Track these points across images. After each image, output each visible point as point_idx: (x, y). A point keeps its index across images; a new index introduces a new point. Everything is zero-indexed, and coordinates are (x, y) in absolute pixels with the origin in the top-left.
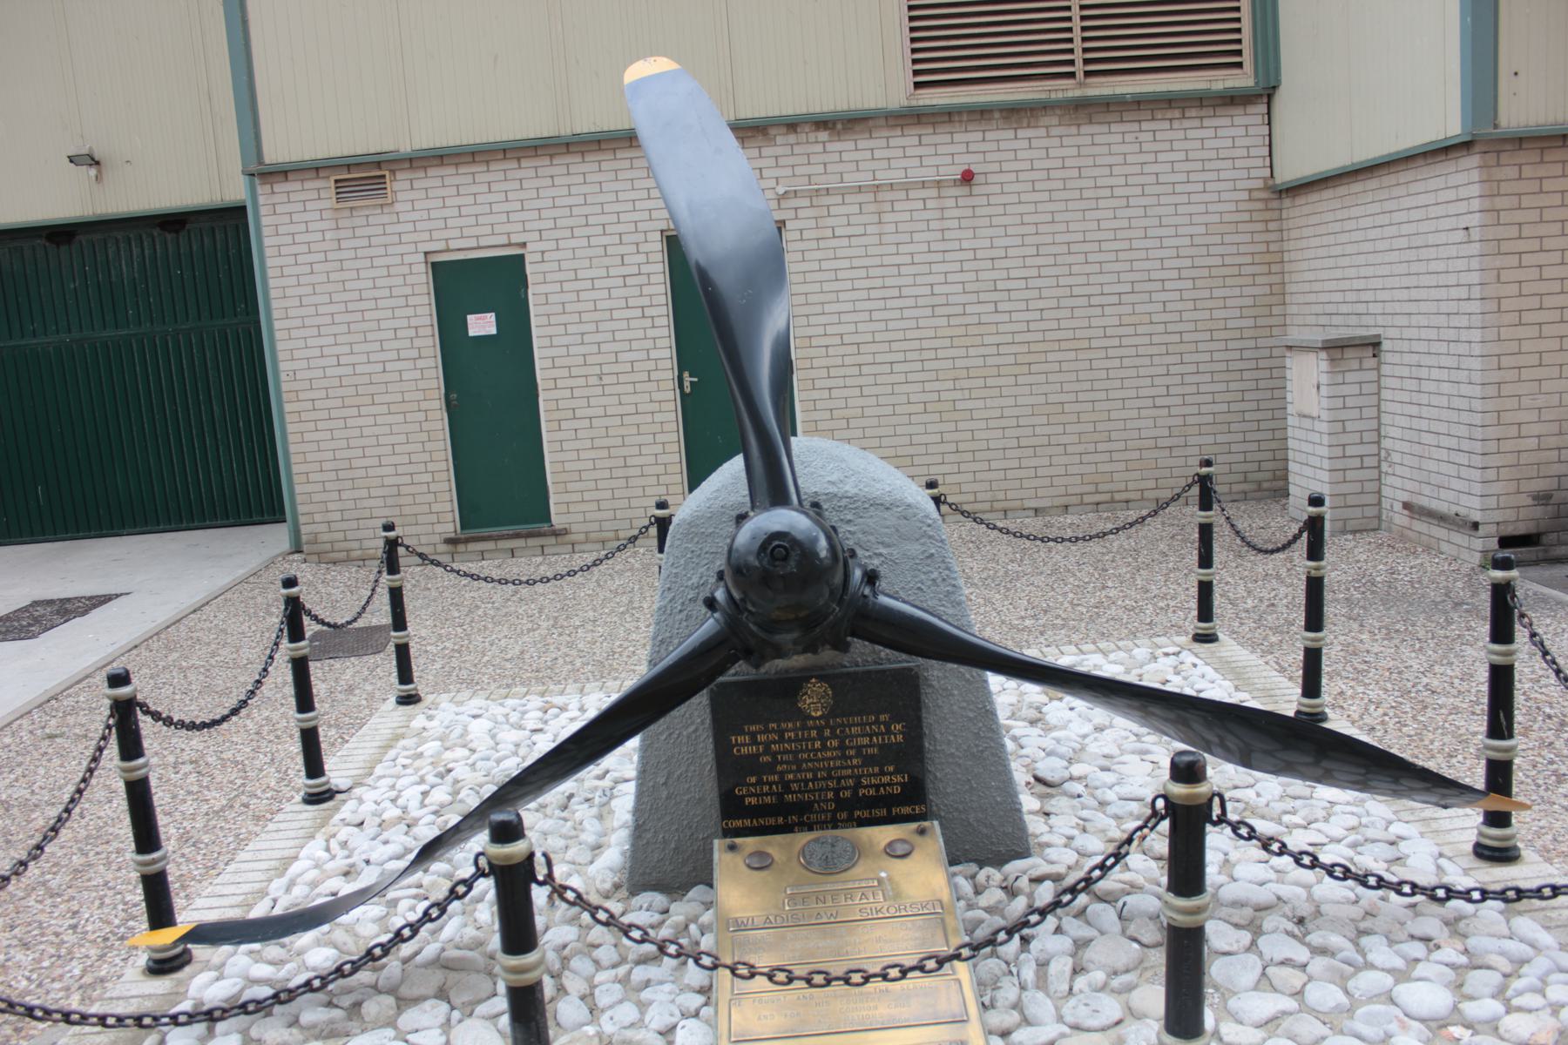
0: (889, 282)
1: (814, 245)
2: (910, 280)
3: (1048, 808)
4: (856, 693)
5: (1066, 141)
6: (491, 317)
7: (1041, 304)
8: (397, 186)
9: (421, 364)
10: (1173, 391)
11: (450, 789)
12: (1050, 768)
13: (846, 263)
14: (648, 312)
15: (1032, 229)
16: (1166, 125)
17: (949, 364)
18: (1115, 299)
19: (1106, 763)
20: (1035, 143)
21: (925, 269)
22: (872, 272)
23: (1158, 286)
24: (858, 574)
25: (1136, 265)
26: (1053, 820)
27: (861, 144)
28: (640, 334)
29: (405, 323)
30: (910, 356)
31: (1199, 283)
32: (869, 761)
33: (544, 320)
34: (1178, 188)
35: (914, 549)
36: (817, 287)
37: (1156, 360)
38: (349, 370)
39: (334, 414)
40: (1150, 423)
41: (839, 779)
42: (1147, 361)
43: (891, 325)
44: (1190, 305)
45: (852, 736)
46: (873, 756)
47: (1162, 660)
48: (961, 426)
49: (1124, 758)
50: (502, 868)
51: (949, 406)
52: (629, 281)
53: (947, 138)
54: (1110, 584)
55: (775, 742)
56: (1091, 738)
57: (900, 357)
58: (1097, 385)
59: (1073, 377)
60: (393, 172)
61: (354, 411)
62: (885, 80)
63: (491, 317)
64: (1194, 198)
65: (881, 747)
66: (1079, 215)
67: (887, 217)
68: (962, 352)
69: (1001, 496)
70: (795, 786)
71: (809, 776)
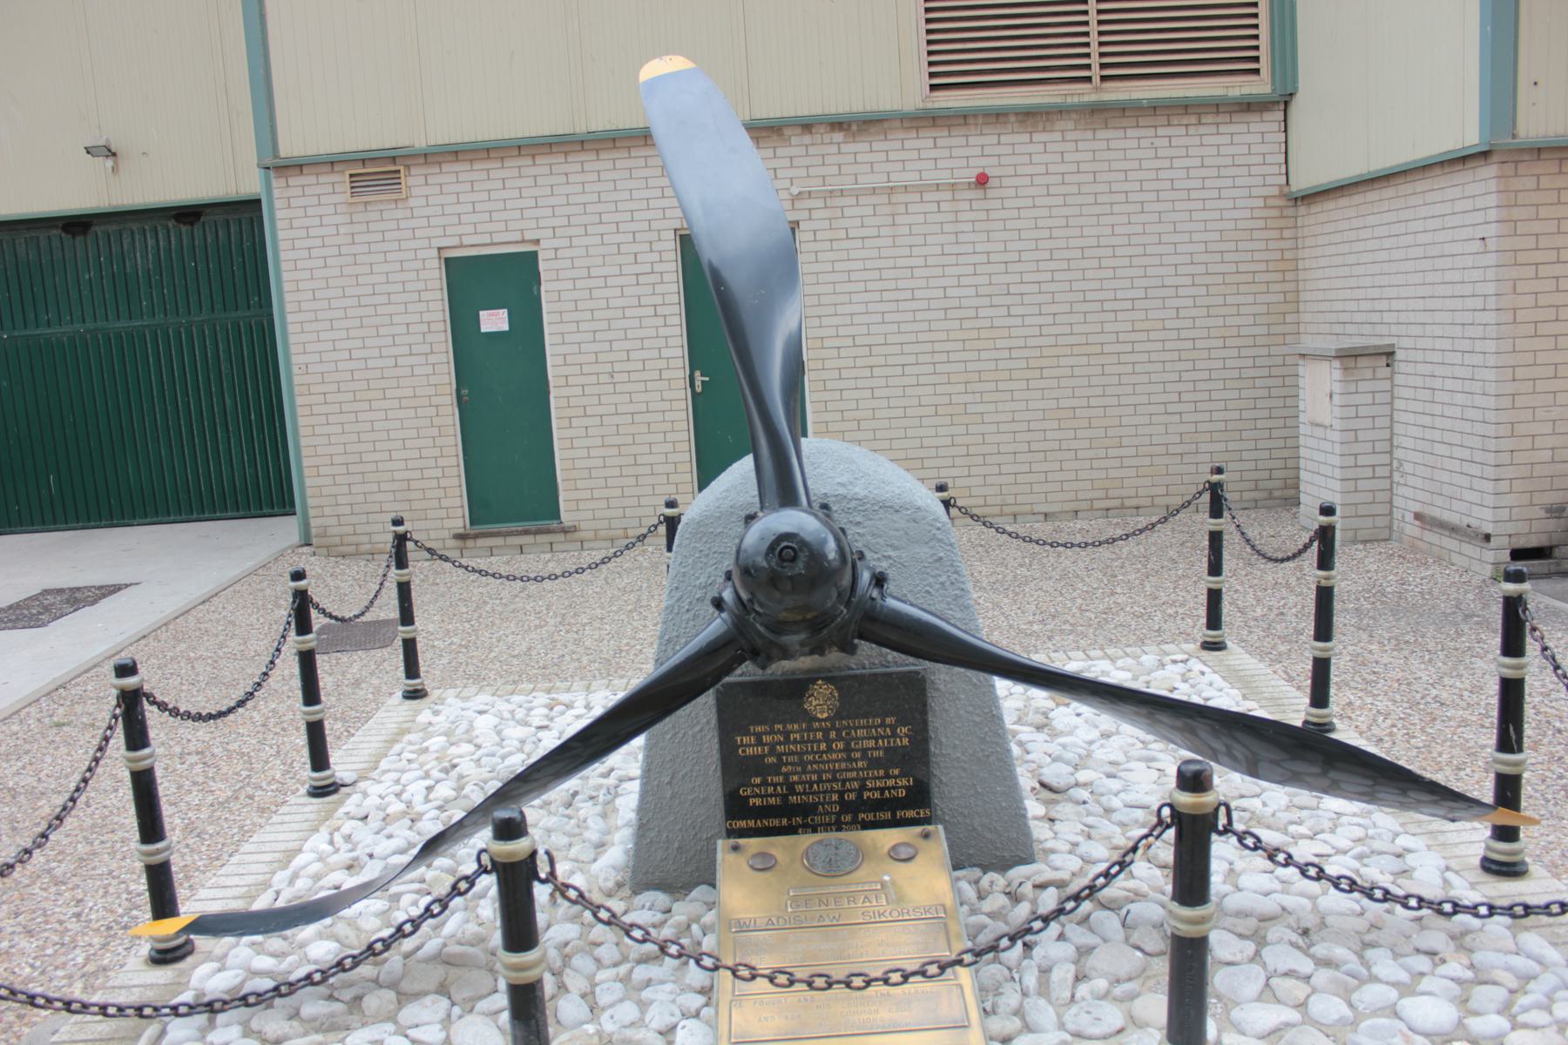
0: (901, 284)
1: (827, 245)
3: (1053, 814)
4: (860, 694)
5: (1081, 145)
8: (411, 181)
9: (432, 359)
12: (1056, 774)
13: (859, 265)
16: (1182, 131)
17: (961, 367)
18: (1128, 305)
19: (1112, 769)
22: (885, 274)
23: (1171, 292)
24: (866, 576)
25: (1150, 271)
26: (1058, 826)
27: (876, 146)
28: (653, 333)
29: (417, 318)
32: (874, 763)
35: (923, 552)
37: (1169, 366)
38: (361, 364)
41: (844, 781)
45: (857, 738)
48: (972, 429)
49: (1131, 765)
50: (505, 866)
52: (642, 279)
53: (962, 141)
54: (1119, 590)
55: (780, 743)
57: (912, 359)
60: (408, 167)
64: (1209, 205)
65: (887, 750)
67: (899, 220)
69: (1011, 500)
70: (799, 788)
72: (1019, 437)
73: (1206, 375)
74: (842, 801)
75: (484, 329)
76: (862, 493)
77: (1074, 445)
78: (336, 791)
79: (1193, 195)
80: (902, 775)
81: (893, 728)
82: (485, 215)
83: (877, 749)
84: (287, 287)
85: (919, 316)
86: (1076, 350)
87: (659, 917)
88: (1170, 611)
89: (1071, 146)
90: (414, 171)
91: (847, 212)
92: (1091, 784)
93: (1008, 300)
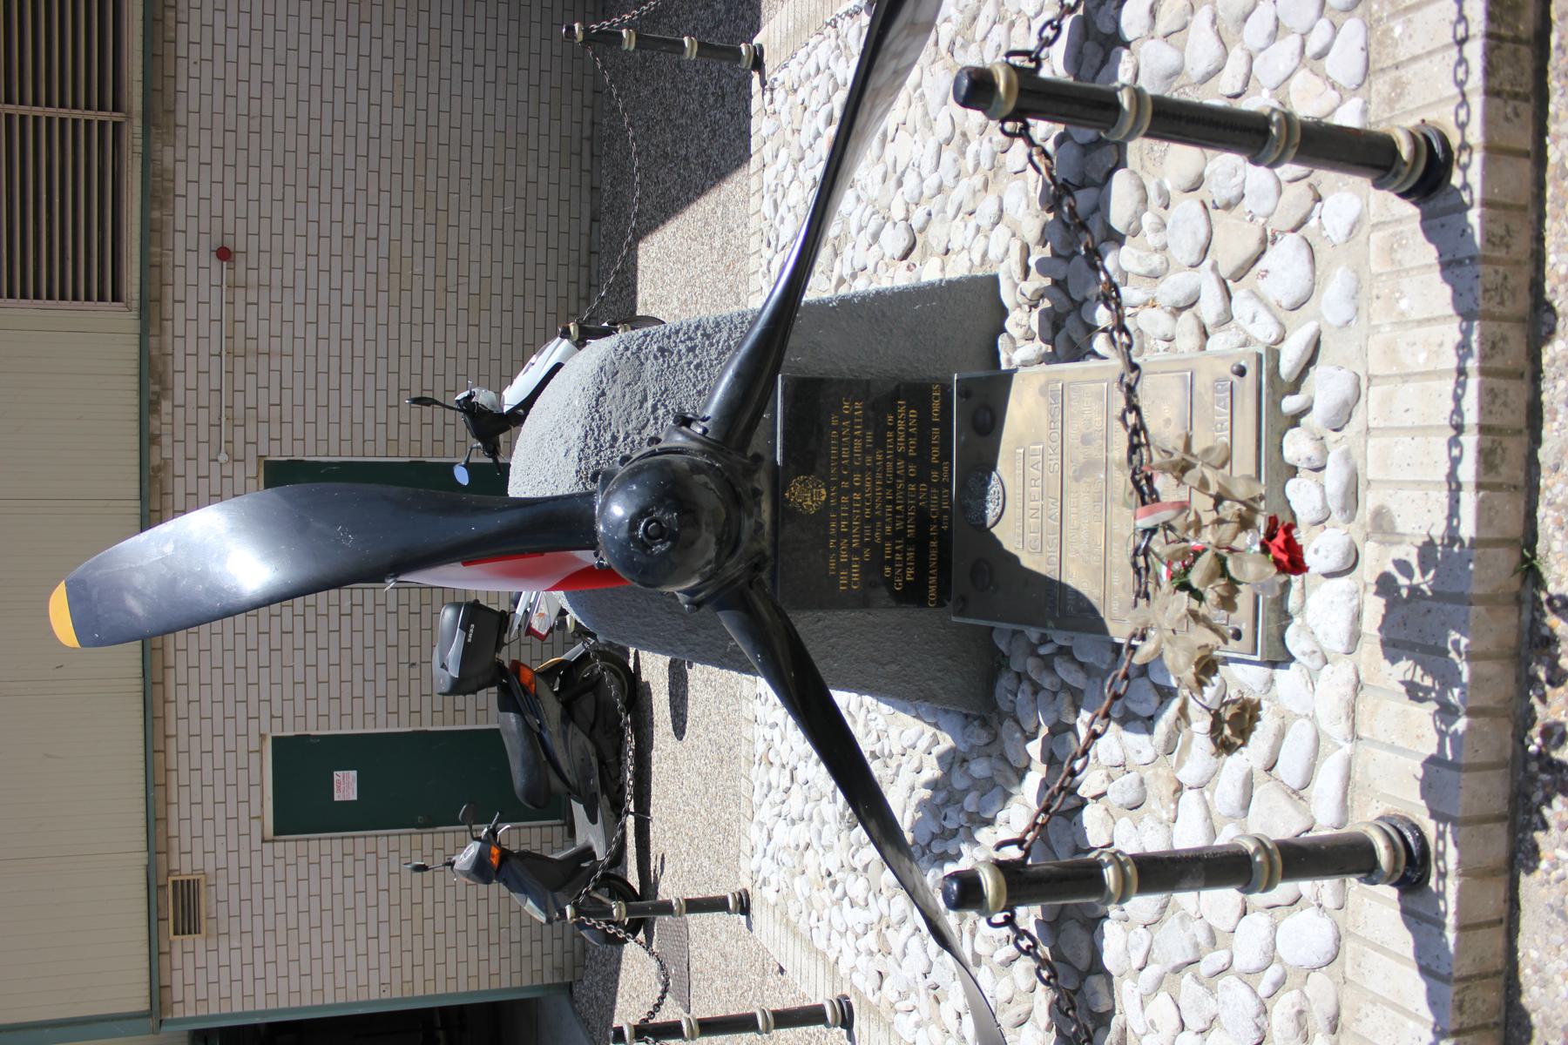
0: (335, 351)
1: (287, 428)
2: (335, 328)
3: (942, 249)
4: (806, 449)
6: (338, 776)
7: (373, 190)
8: (186, 869)
9: (383, 852)
10: (480, 61)
11: (852, 876)
12: (894, 241)
13: (311, 395)
16: (182, 28)
17: (429, 296)
19: (892, 182)
21: (323, 310)
22: (323, 367)
24: (679, 440)
25: (340, 82)
26: (955, 246)
27: (179, 366)
30: (417, 336)
31: (365, 17)
32: (880, 442)
33: (346, 720)
34: (257, 24)
35: (651, 367)
38: (384, 927)
39: (429, 945)
40: (512, 88)
41: (896, 476)
43: (382, 353)
44: (388, 30)
45: (851, 458)
46: (874, 436)
47: (777, 105)
49: (889, 161)
50: (1010, 898)
51: (474, 300)
52: (310, 627)
53: (179, 272)
54: (683, 152)
55: (850, 543)
56: (861, 193)
57: (417, 346)
60: (170, 872)
62: (108, 331)
63: (338, 776)
65: (866, 427)
67: (264, 347)
68: (418, 280)
69: (574, 255)
71: (889, 508)
72: (509, 241)
73: (457, 35)
76: (579, 431)
77: (521, 182)
78: (850, 1006)
79: (257, 24)
81: (845, 417)
82: (229, 795)
84: (295, 1003)
85: (371, 335)
86: (420, 171)
87: (1025, 686)
88: (711, 101)
90: (175, 866)
92: (907, 204)
93: (360, 239)
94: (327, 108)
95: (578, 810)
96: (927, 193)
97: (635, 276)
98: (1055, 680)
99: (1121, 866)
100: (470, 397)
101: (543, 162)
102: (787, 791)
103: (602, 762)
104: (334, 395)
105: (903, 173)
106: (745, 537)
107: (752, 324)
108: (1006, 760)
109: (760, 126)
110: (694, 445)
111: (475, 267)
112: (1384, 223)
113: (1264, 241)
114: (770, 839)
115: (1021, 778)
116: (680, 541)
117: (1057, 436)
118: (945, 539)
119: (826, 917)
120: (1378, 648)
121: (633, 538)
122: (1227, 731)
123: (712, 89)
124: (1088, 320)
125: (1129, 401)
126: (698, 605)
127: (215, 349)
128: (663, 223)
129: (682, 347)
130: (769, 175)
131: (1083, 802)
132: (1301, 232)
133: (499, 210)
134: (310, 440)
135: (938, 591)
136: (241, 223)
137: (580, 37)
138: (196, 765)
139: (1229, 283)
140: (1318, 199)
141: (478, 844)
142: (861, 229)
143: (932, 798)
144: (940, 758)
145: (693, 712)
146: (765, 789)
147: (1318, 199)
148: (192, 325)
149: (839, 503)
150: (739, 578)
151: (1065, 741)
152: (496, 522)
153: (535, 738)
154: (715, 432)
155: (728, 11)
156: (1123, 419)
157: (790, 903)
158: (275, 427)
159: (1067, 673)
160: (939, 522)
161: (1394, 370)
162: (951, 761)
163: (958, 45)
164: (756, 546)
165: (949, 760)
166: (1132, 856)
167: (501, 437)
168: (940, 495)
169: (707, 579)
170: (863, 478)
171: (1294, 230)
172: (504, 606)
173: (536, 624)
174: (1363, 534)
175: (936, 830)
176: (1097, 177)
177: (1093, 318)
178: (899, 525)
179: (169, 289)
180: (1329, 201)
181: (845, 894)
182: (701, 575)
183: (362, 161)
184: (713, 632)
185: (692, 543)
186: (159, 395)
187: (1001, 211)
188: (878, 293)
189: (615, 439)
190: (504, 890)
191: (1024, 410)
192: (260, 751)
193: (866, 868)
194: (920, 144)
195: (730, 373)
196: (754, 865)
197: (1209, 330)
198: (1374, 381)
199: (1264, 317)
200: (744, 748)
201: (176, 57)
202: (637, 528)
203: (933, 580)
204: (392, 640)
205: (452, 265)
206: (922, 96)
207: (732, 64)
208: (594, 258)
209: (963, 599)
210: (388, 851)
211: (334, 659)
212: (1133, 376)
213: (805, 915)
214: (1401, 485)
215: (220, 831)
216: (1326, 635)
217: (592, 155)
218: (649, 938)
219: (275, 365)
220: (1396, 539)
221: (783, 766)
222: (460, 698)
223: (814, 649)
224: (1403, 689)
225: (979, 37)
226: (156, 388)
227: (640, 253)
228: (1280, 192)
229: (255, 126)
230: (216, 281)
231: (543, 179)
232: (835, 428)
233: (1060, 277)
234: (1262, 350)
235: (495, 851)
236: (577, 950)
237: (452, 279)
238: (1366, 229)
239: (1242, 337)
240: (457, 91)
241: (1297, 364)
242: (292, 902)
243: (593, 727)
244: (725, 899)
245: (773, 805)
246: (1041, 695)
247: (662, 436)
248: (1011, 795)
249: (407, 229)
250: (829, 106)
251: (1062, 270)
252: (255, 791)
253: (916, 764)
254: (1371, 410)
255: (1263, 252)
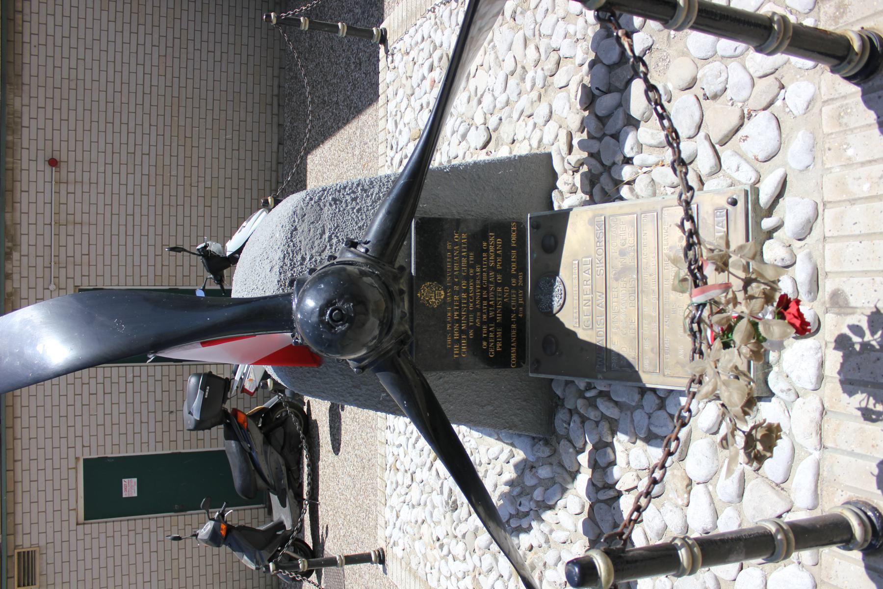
0: (123, 222)
1: (93, 268)
2: (123, 208)
3: (510, 140)
4: (432, 267)
5: (34, 94)
6: (125, 482)
7: (146, 125)
8: (27, 544)
9: (153, 528)
11: (454, 541)
13: (108, 248)
14: (130, 379)
15: (95, 125)
16: (27, 25)
17: (181, 188)
18: (147, 77)
19: (474, 101)
20: (33, 115)
21: (116, 197)
23: (141, 48)
24: (349, 256)
25: (126, 60)
26: (519, 137)
28: (144, 385)
29: (125, 539)
30: (173, 212)
31: (142, 21)
32: (479, 260)
33: (130, 447)
35: (327, 212)
36: (122, 269)
37: (191, 56)
38: (154, 575)
41: (489, 282)
42: (190, 62)
43: (152, 223)
45: (460, 270)
46: (475, 256)
47: (396, 63)
48: (221, 185)
51: (208, 191)
52: (108, 390)
54: (335, 99)
57: (173, 219)
58: (203, 96)
59: (196, 111)
60: (16, 547)
61: (182, 571)
63: (125, 482)
64: (82, 15)
65: (469, 250)
66: (88, 92)
67: (78, 219)
68: (173, 179)
69: (268, 165)
70: (492, 314)
72: (229, 156)
74: (502, 285)
75: (135, 494)
76: (280, 254)
77: (236, 121)
79: (74, 24)
80: (487, 241)
81: (456, 244)
83: (468, 257)
85: (145, 212)
86: (175, 113)
87: (576, 418)
88: (353, 67)
89: (33, 101)
90: (19, 542)
91: (70, 253)
94: (118, 75)
95: (274, 499)
96: (499, 106)
97: (305, 176)
98: (598, 414)
99: (690, 548)
100: (206, 247)
101: (250, 109)
102: (409, 487)
103: (289, 469)
104: (122, 248)
105: (482, 96)
106: (396, 321)
107: (395, 182)
108: (563, 467)
109: (385, 77)
110: (360, 260)
111: (208, 171)
112: (832, 99)
113: (742, 117)
114: (398, 517)
115: (574, 478)
116: (355, 321)
117: (602, 251)
118: (521, 322)
119: (437, 567)
120: (839, 385)
121: (321, 321)
122: (759, 447)
123: (353, 60)
124: (616, 177)
125: (686, 212)
126: (363, 369)
127: (48, 221)
128: (323, 142)
129: (348, 198)
130: (391, 106)
131: (619, 494)
132: (769, 110)
133: (223, 138)
134: (108, 276)
135: (517, 357)
136: (64, 144)
137: (274, 21)
138: (34, 478)
139: (717, 147)
140: (782, 87)
141: (213, 522)
142: (453, 132)
143: (509, 493)
144: (516, 466)
145: (345, 438)
146: (394, 486)
147: (782, 87)
148: (33, 206)
149: (453, 300)
150: (391, 350)
151: (605, 453)
152: (223, 315)
153: (247, 456)
154: (374, 251)
155: (363, 13)
156: (682, 226)
157: (412, 557)
158: (85, 268)
159: (605, 408)
160: (517, 312)
161: (844, 197)
162: (523, 468)
163: (518, 12)
164: (402, 328)
165: (522, 467)
166: (696, 539)
167: (225, 271)
168: (517, 294)
169: (371, 350)
170: (468, 283)
171: (765, 109)
172: (227, 375)
173: (247, 385)
174: (824, 308)
175: (513, 512)
176: (620, 85)
177: (620, 176)
178: (492, 314)
179: (18, 184)
180: (791, 88)
181: (450, 552)
182: (368, 347)
183: (139, 108)
184: (370, 387)
185: (364, 324)
186: (11, 249)
187: (551, 113)
188: (475, 163)
189: (303, 259)
190: (229, 550)
191: (578, 236)
192: (76, 468)
193: (464, 536)
194: (493, 77)
195: (381, 216)
196: (388, 533)
197: (704, 179)
198: (828, 206)
199: (745, 167)
200: (380, 460)
201: (23, 42)
202: (325, 314)
203: (513, 350)
204: (159, 398)
205: (195, 170)
206: (494, 47)
207: (368, 39)
208: (280, 166)
209: (538, 362)
210: (158, 526)
211: (123, 410)
212: (689, 194)
213: (422, 565)
214: (852, 274)
215: (50, 519)
216: (799, 378)
217: (279, 105)
218: (319, 577)
219: (85, 230)
220: (849, 311)
221: (406, 471)
222: (200, 432)
223: (440, 396)
224: (859, 413)
225: (532, 6)
226: (10, 244)
227: (308, 161)
228: (753, 85)
229: (73, 86)
230: (48, 179)
231: (249, 119)
232: (449, 251)
233: (594, 150)
234: (748, 188)
235: (223, 526)
236: (274, 583)
237: (194, 179)
238: (818, 104)
239: (729, 181)
240: (197, 66)
241: (771, 197)
242: (96, 562)
243: (283, 448)
244: (369, 555)
245: (399, 496)
246: (587, 423)
247: (337, 255)
248: (567, 489)
249: (167, 148)
250: (431, 60)
251: (595, 146)
252: (72, 493)
253: (498, 470)
254: (828, 222)
255: (742, 125)
